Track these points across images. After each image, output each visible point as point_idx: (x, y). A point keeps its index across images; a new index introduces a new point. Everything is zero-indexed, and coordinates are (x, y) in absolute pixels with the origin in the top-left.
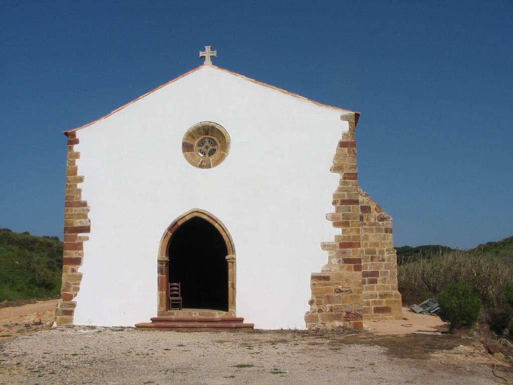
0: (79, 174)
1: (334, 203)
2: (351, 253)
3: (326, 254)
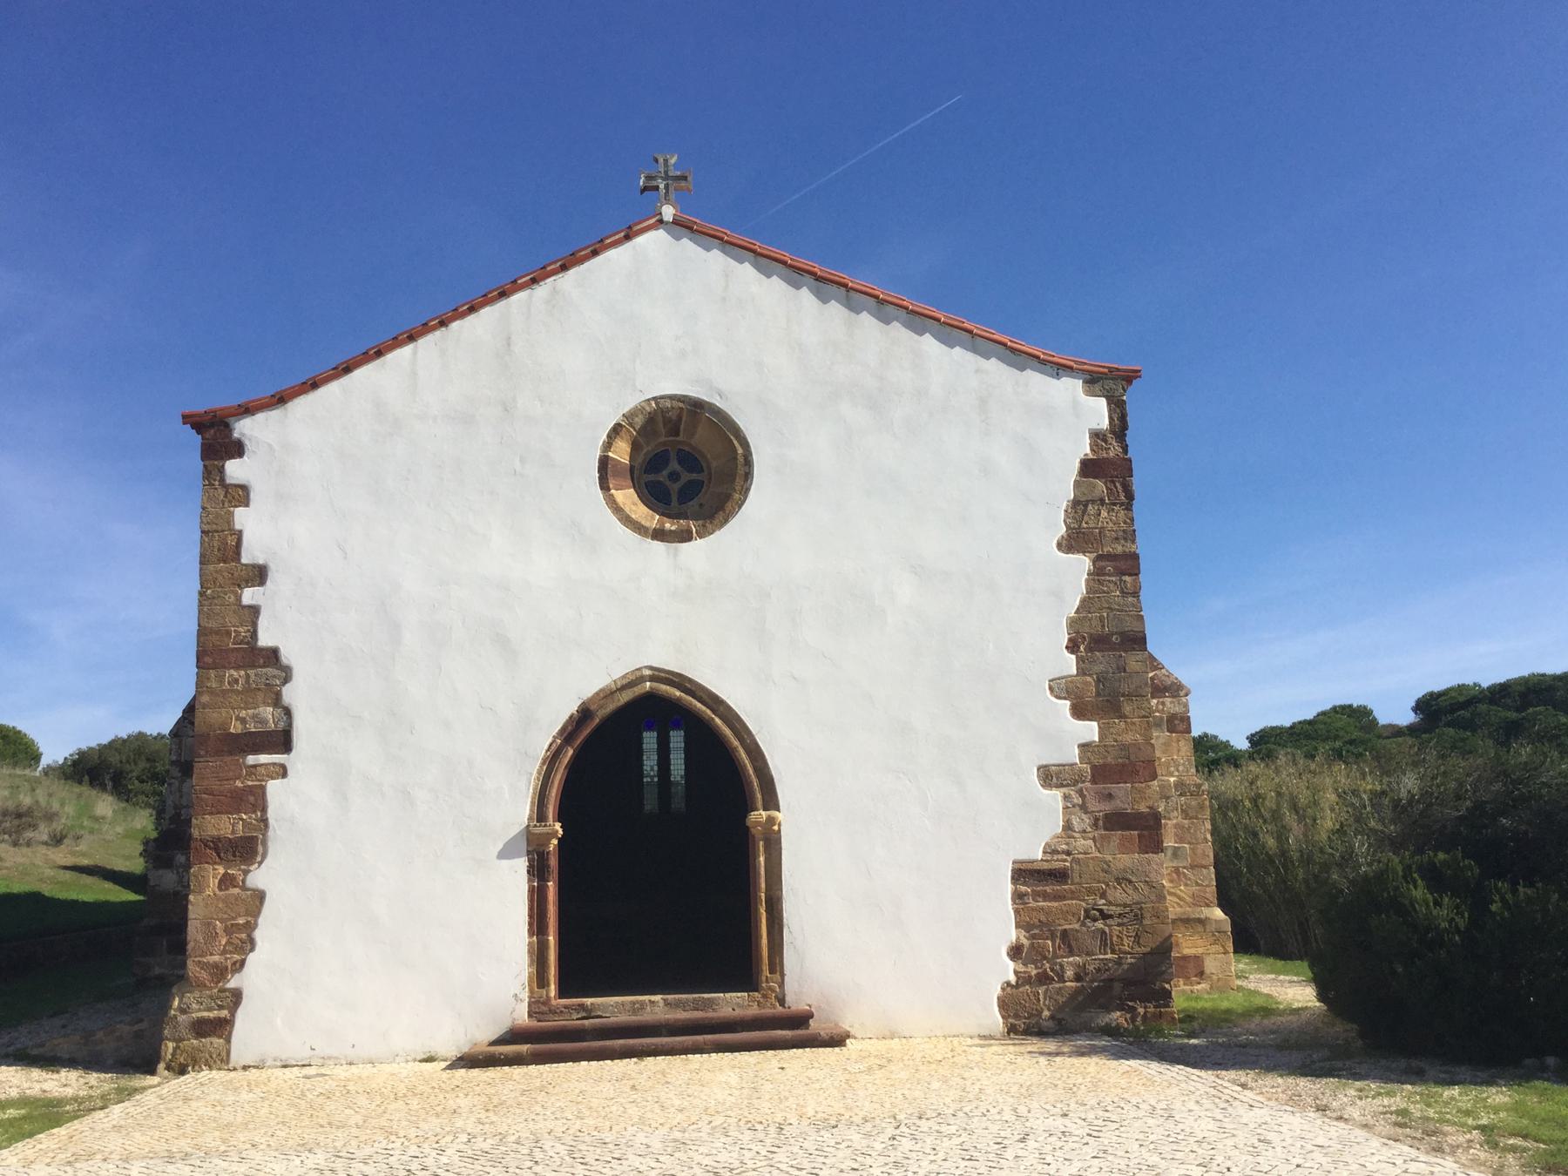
1: (1072, 647)
2: (1124, 796)
3: (1054, 799)
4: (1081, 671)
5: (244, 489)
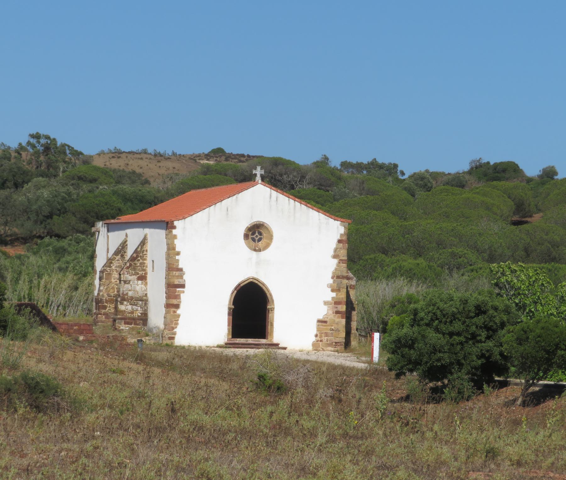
0: (177, 249)
1: (332, 278)
4: (334, 283)
5: (16, 152)
